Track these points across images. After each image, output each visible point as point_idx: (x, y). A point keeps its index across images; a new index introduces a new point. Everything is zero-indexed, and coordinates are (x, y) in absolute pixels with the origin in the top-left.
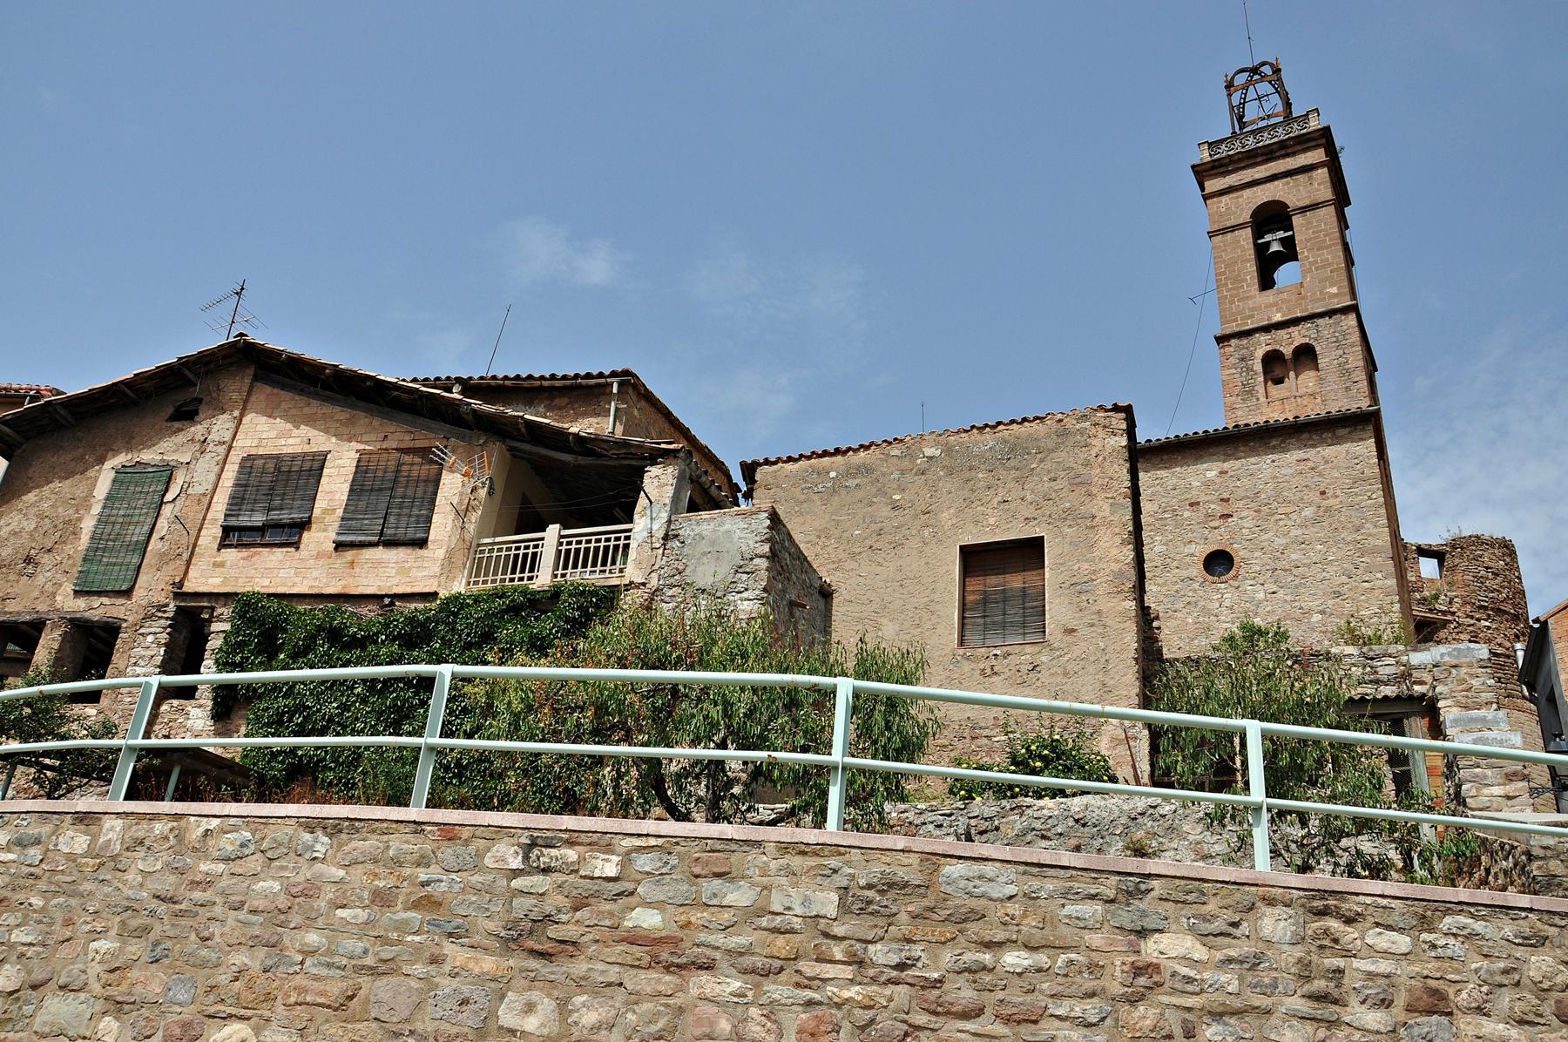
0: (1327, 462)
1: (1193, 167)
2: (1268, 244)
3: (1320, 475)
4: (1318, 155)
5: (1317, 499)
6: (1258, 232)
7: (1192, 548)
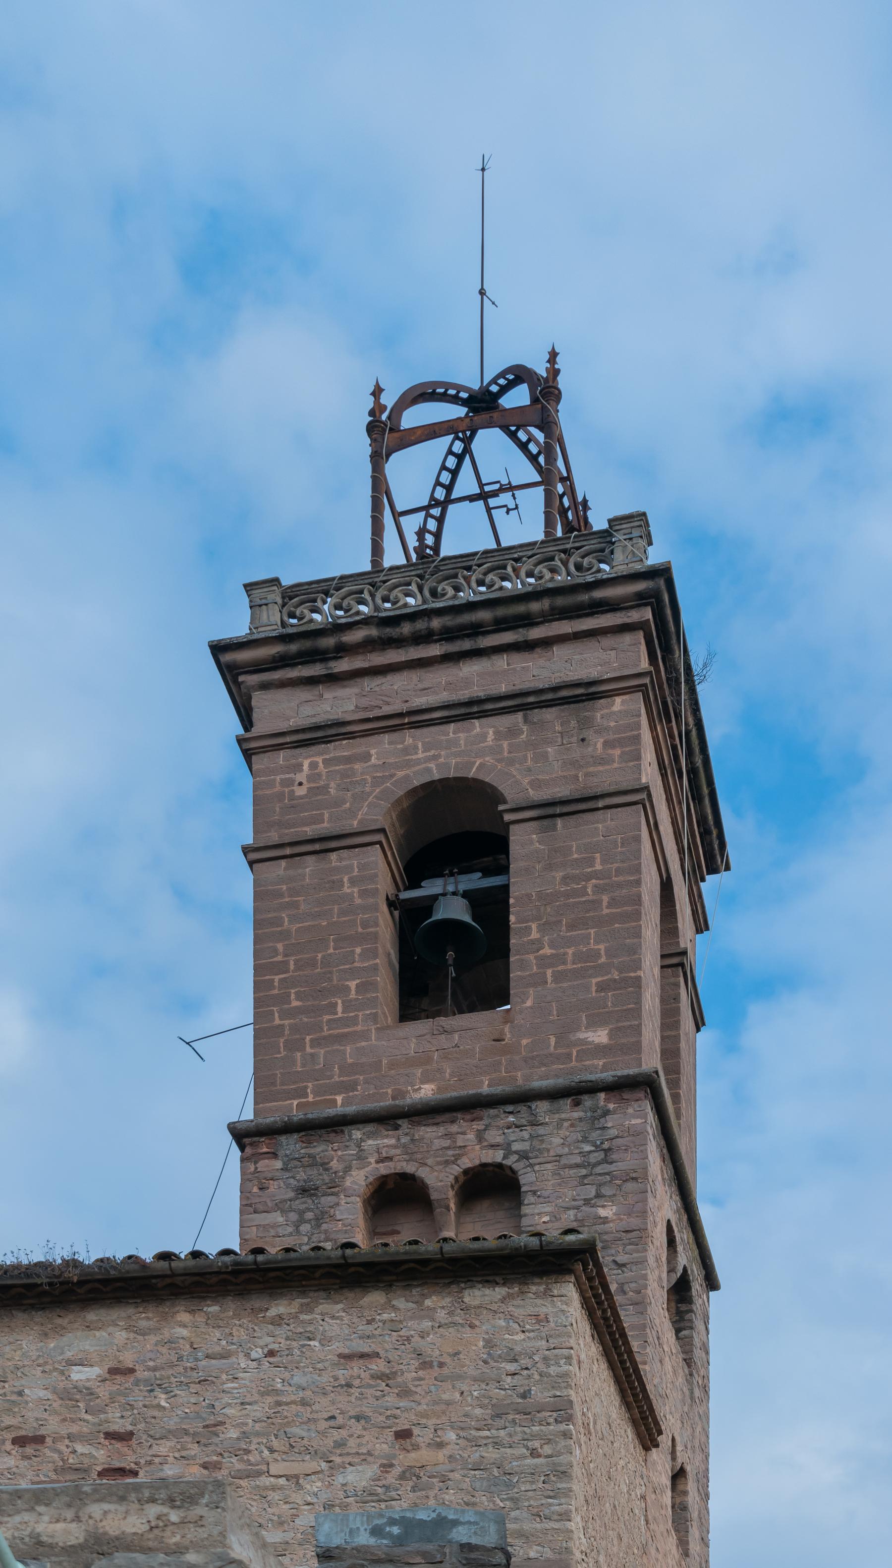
0: (426, 1365)
1: (218, 649)
2: (427, 905)
3: (405, 1393)
5: (383, 1445)
6: (418, 864)
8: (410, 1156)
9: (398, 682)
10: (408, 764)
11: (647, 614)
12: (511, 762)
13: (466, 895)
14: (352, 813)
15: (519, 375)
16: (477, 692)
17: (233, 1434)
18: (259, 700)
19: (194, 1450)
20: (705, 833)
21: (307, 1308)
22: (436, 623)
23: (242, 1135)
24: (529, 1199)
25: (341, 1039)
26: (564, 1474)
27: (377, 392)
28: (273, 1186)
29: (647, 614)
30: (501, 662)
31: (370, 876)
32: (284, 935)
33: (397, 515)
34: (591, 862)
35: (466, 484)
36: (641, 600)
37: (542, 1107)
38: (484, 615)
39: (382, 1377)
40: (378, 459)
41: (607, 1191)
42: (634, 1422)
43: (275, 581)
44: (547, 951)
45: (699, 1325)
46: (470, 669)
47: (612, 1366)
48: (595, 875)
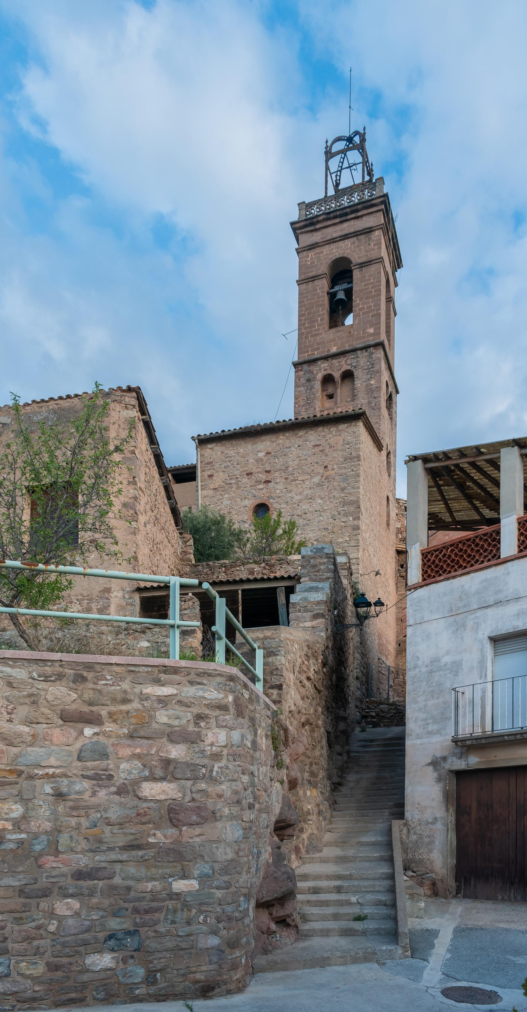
0: (331, 447)
3: (326, 455)
4: (378, 219)
5: (321, 470)
6: (334, 281)
7: (246, 502)
8: (331, 369)
9: (329, 230)
10: (332, 254)
11: (383, 207)
12: (354, 251)
13: (344, 290)
14: (320, 268)
15: (357, 133)
16: (346, 232)
17: (291, 469)
18: (300, 237)
19: (283, 474)
20: (397, 259)
21: (306, 433)
22: (338, 213)
23: (295, 365)
24: (356, 379)
25: (316, 335)
26: (358, 476)
27: (327, 142)
28: (302, 379)
29: (383, 207)
30: (352, 222)
31: (323, 285)
32: (305, 305)
33: (331, 174)
34: (370, 279)
35: (346, 165)
36: (382, 203)
37: (359, 352)
38: (348, 210)
39: (322, 451)
40: (327, 161)
41: (373, 376)
42: (377, 446)
43: (304, 202)
44: (361, 306)
45: (394, 406)
46: (345, 225)
47: (371, 435)
48: (371, 284)
